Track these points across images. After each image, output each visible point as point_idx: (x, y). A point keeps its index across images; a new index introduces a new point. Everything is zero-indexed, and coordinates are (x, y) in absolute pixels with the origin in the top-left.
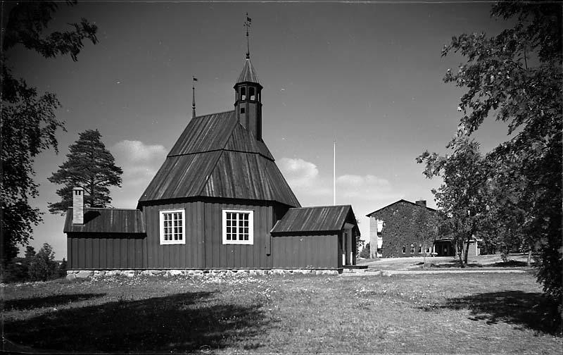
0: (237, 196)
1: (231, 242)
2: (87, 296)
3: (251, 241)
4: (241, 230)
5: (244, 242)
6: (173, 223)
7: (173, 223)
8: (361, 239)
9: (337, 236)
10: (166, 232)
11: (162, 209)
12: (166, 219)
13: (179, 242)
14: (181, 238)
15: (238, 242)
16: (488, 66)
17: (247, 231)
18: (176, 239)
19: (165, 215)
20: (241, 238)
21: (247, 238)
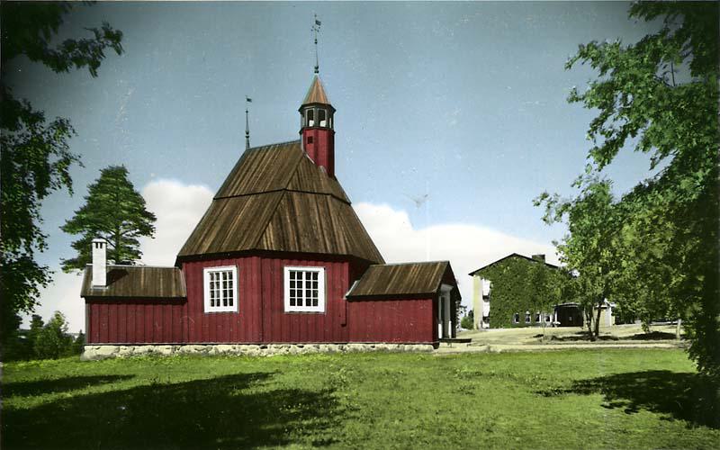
1: (296, 309)
2: (111, 379)
3: (321, 308)
10: (213, 296)
14: (231, 304)
18: (225, 305)
20: (308, 304)
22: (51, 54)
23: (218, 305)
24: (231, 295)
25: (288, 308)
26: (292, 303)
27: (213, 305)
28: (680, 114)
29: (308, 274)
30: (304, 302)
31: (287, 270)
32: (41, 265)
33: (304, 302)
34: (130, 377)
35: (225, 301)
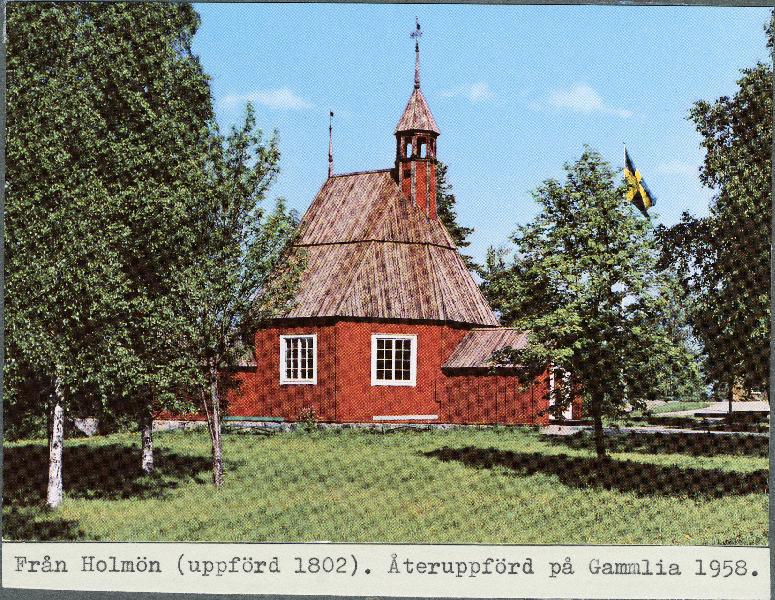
0: (393, 315)
1: (384, 382)
2: (474, 457)
3: (412, 382)
4: (389, 354)
5: (402, 382)
6: (300, 354)
7: (300, 354)
8: (768, 550)
9: (4, 586)
10: (289, 366)
11: (375, 332)
12: (289, 346)
13: (307, 381)
14: (311, 376)
15: (394, 382)
16: (122, 157)
17: (380, 354)
18: (304, 376)
19: (288, 341)
20: (398, 376)
21: (407, 377)
22: (90, 493)
23: (296, 376)
24: (311, 365)
25: (375, 381)
26: (380, 376)
27: (289, 376)
28: (22, 481)
29: (399, 343)
30: (299, 374)
31: (374, 338)
32: (677, 220)
33: (299, 374)
34: (446, 454)
35: (303, 372)
